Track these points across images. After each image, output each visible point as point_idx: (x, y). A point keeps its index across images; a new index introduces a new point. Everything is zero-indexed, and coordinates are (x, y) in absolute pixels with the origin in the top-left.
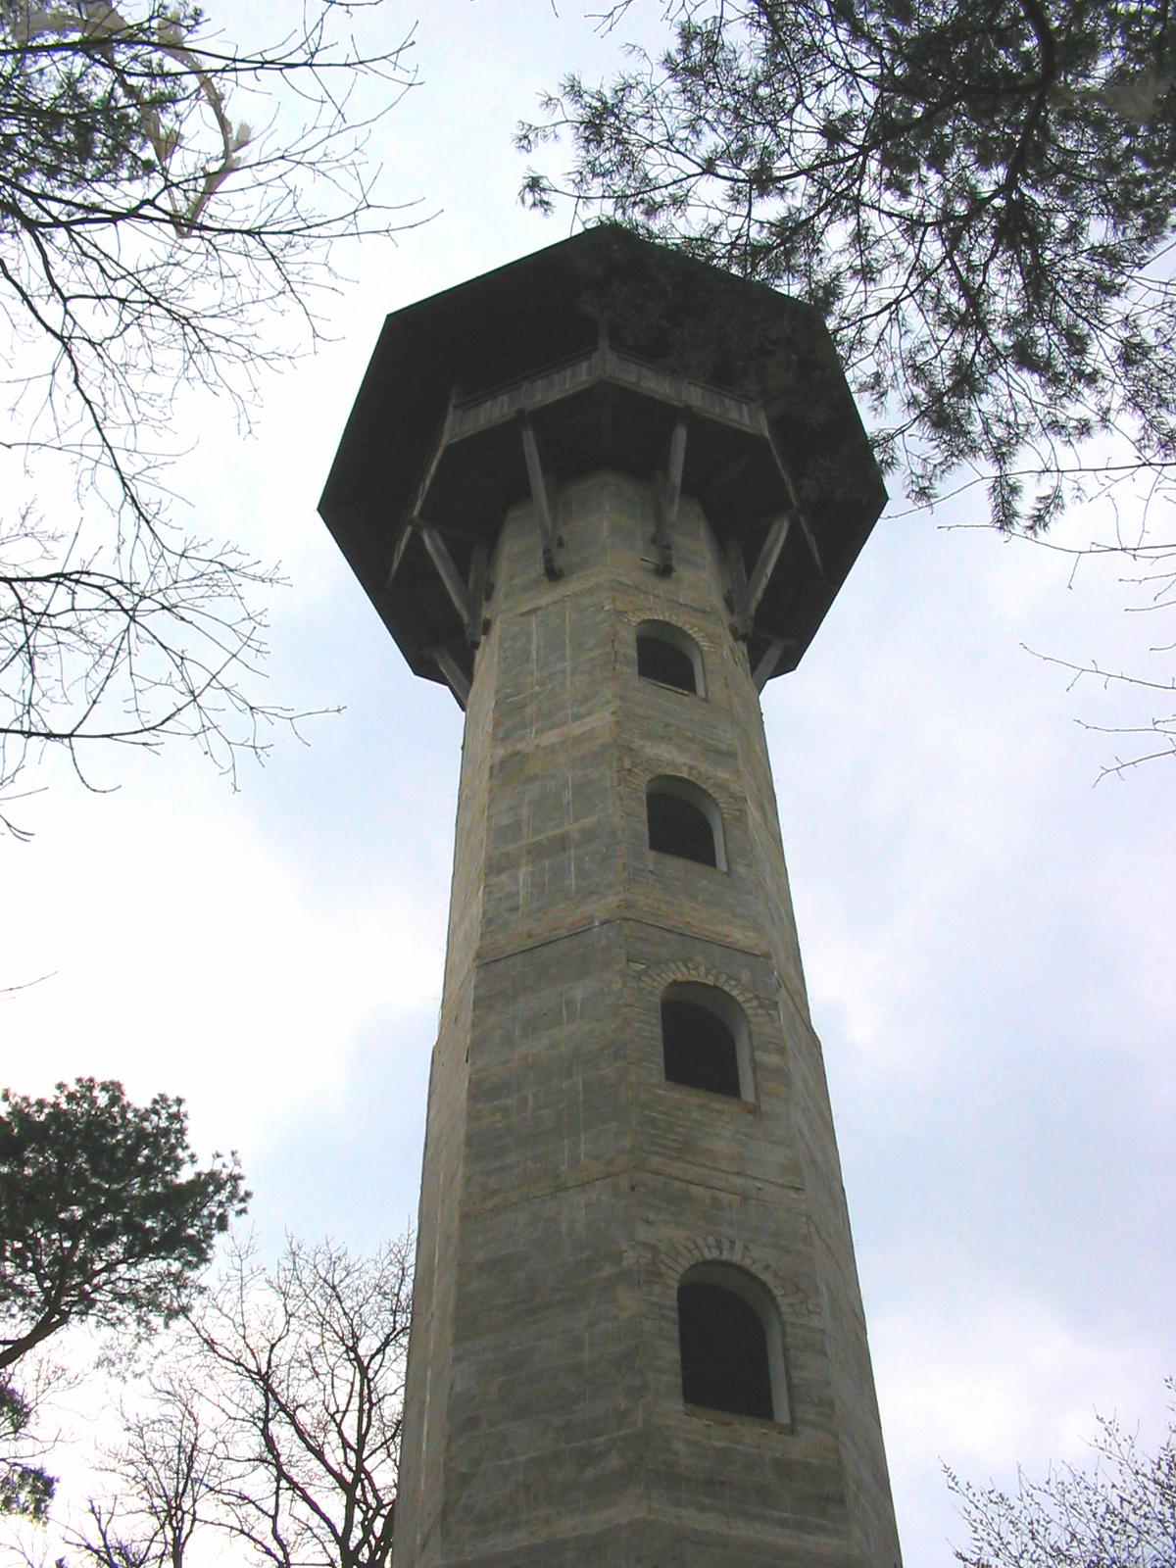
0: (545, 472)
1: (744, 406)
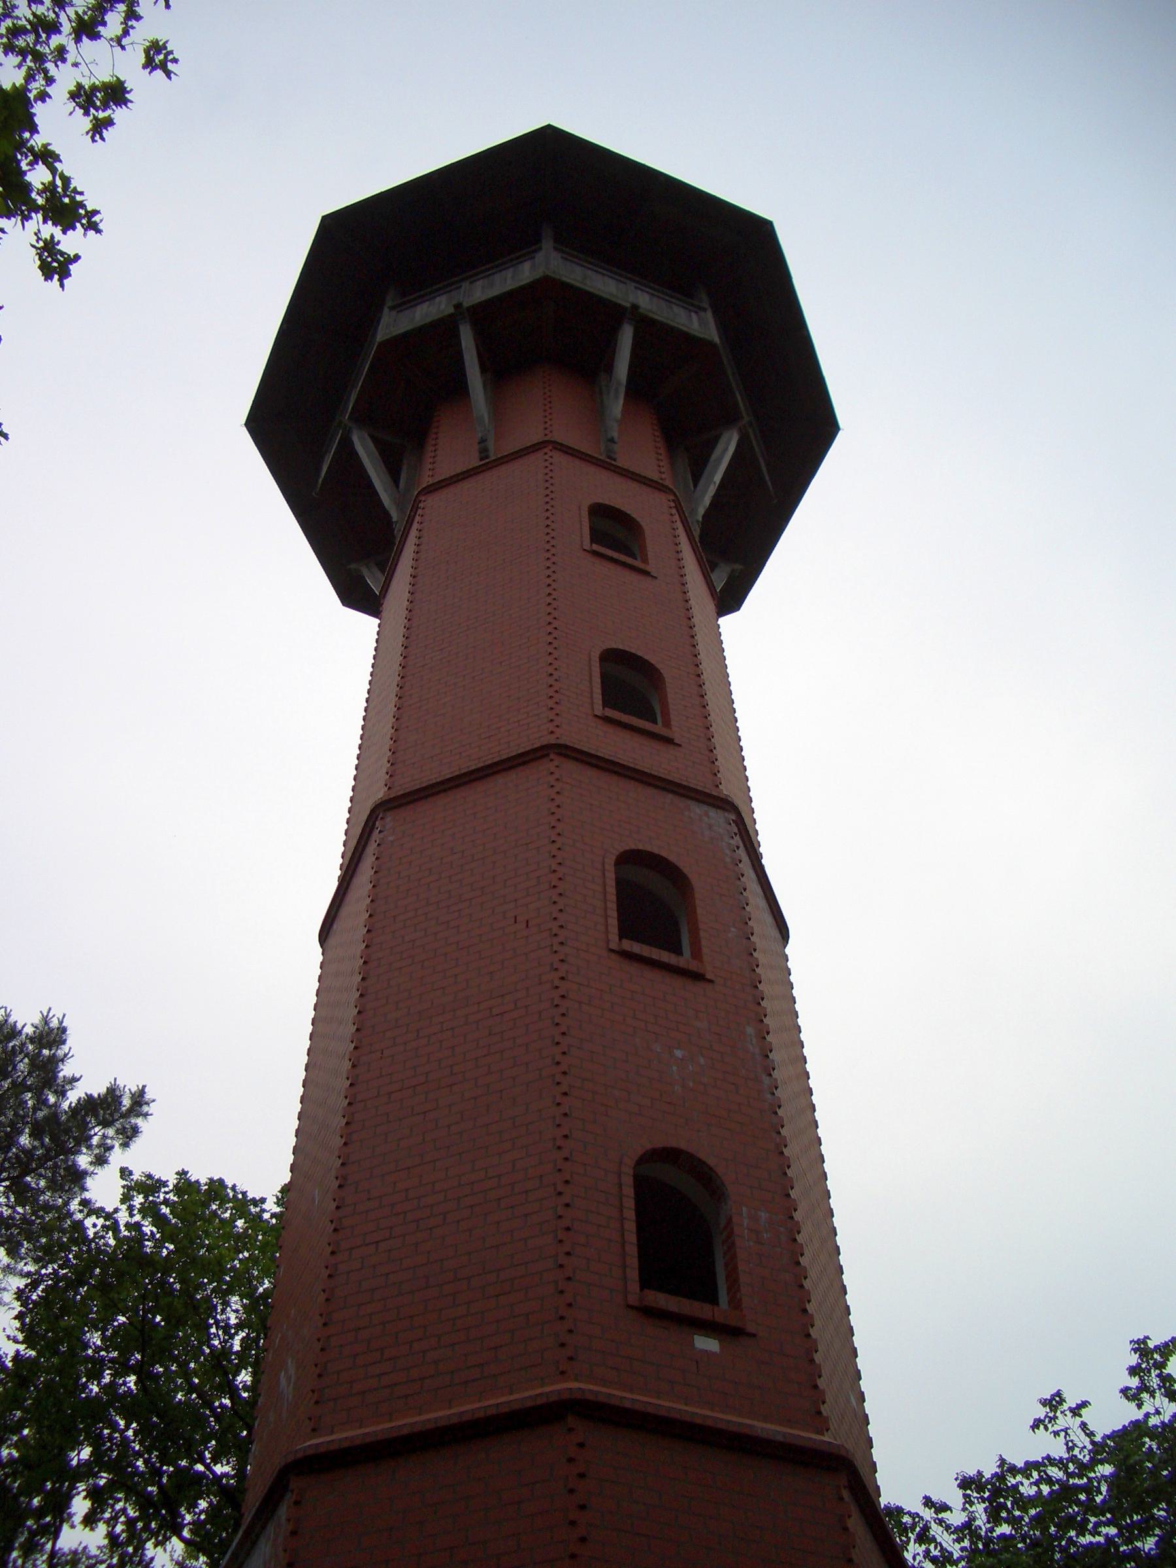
0: (484, 369)
1: (693, 314)
